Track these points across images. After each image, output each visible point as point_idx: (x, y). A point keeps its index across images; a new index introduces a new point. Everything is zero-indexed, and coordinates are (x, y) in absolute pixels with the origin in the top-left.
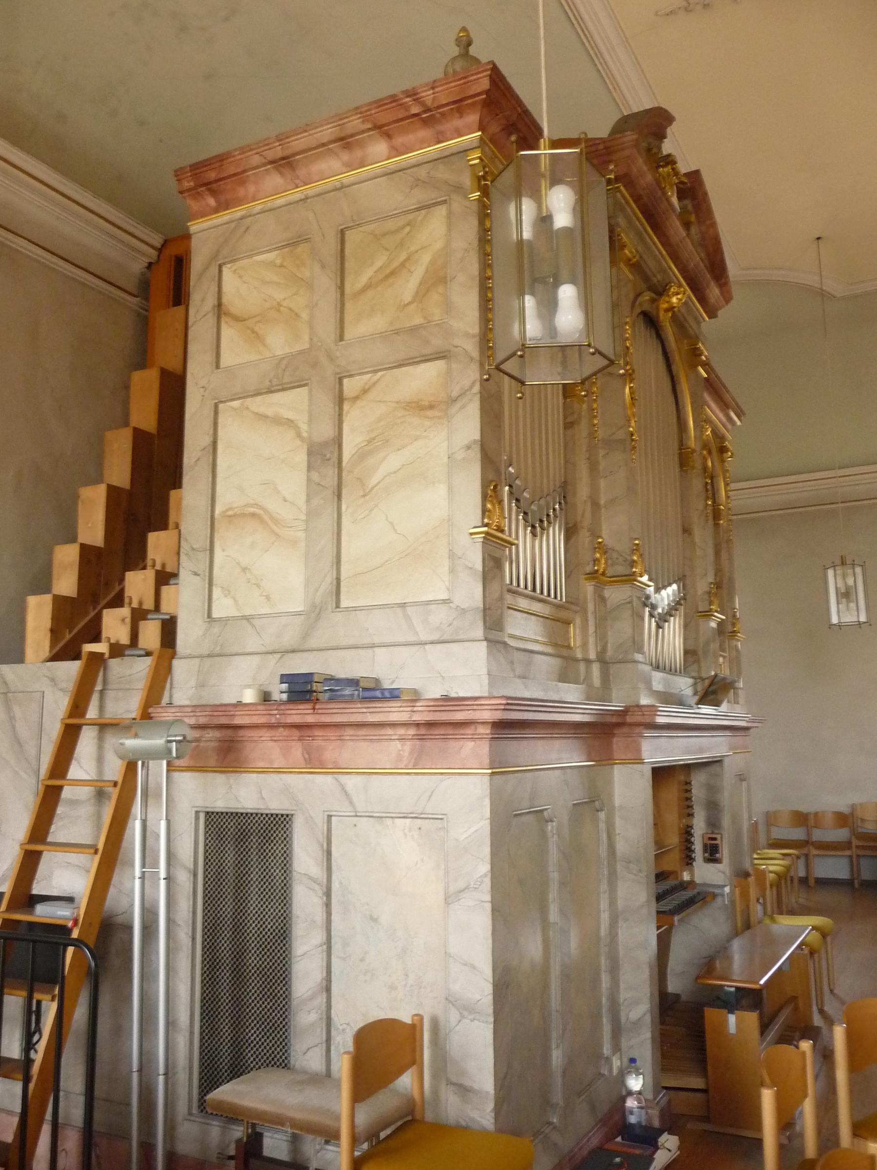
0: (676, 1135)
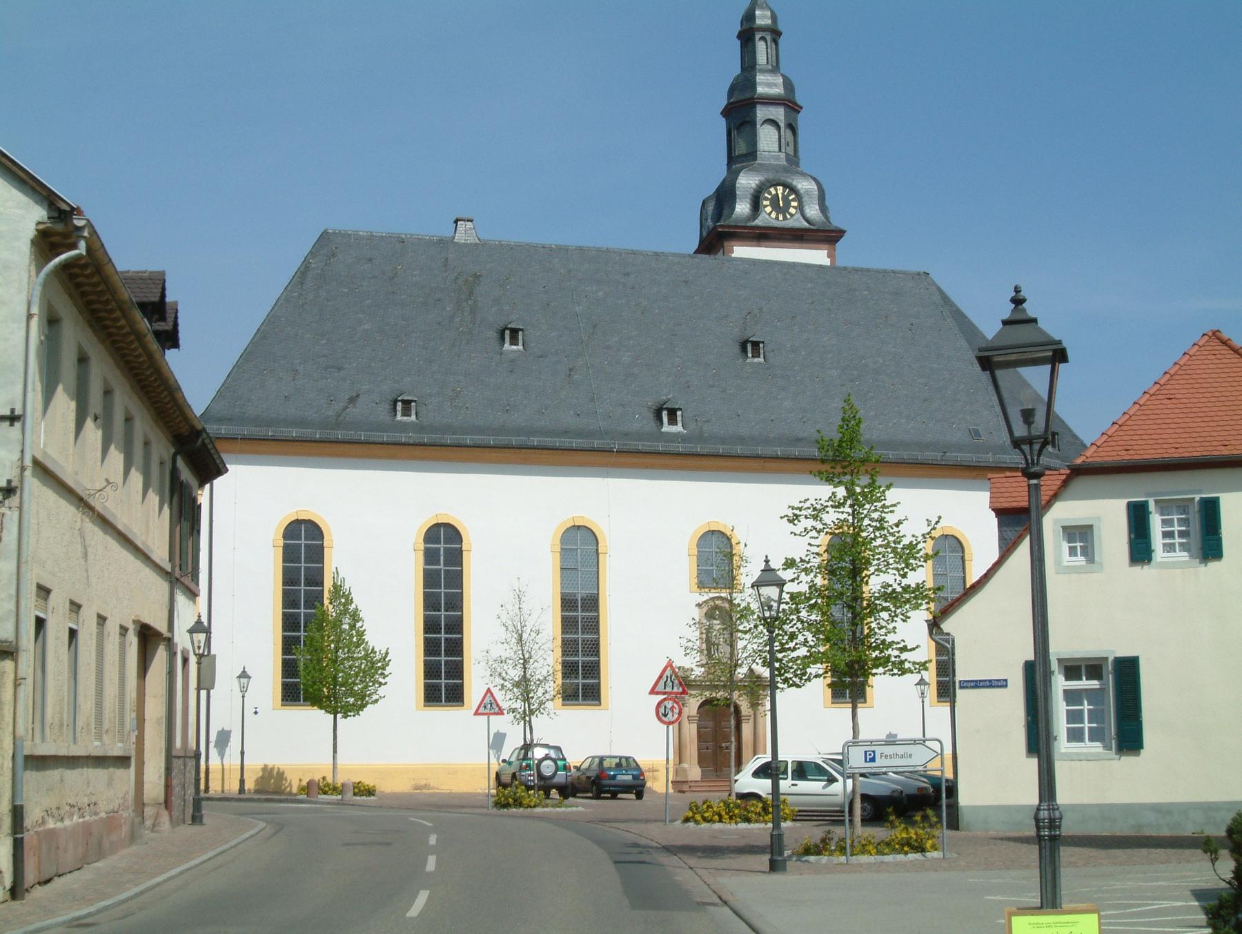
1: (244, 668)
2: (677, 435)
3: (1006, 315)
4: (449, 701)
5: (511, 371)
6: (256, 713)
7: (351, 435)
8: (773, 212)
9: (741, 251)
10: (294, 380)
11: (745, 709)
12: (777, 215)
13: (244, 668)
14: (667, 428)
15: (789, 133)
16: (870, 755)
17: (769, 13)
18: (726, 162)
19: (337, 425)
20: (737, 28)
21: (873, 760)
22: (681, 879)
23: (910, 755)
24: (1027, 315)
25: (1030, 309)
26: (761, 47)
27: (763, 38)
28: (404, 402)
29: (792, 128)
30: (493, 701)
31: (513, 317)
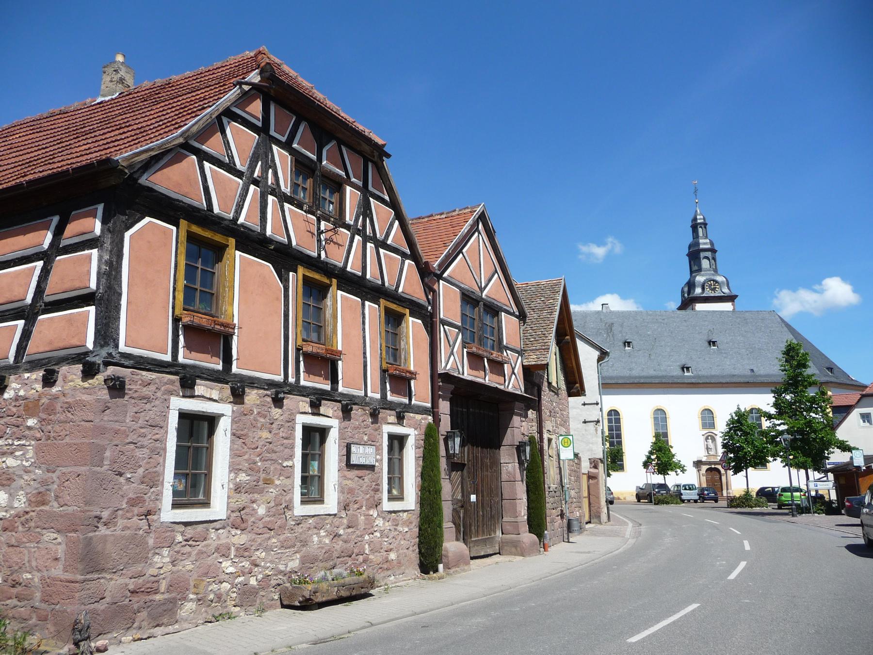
0: (144, 218)
2: (690, 376)
9: (700, 307)
11: (723, 471)
14: (686, 374)
15: (713, 261)
17: (702, 217)
18: (689, 272)
20: (690, 224)
26: (700, 230)
27: (701, 227)
29: (714, 259)
31: (627, 338)
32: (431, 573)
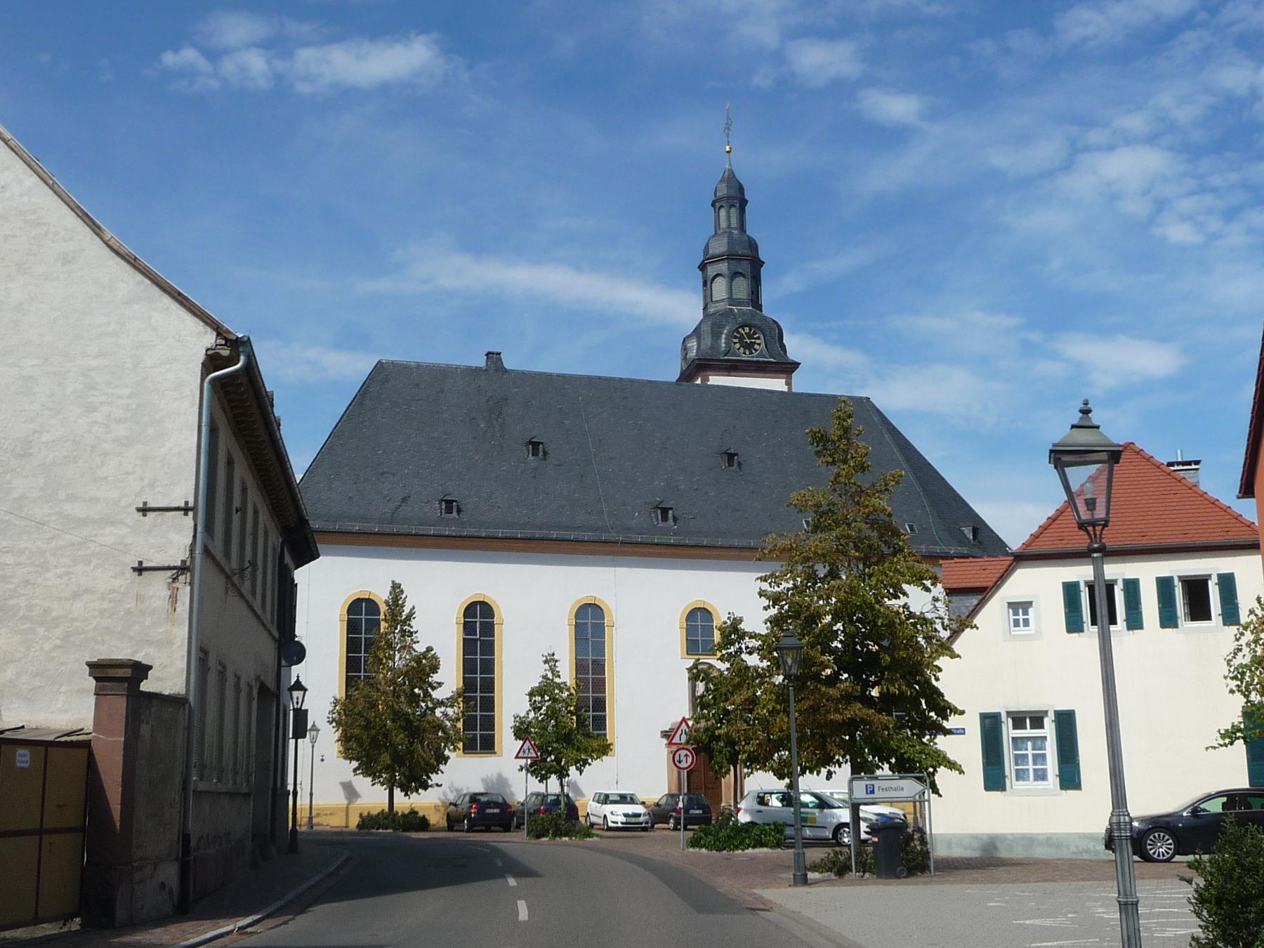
1: (314, 722)
3: (1075, 422)
4: (484, 749)
5: (534, 477)
6: (322, 760)
7: (404, 529)
8: (742, 348)
10: (356, 483)
12: (745, 350)
13: (314, 722)
16: (870, 788)
19: (392, 520)
21: (872, 792)
22: (722, 890)
23: (902, 789)
24: (1092, 422)
25: (1095, 418)
28: (446, 501)
30: (531, 747)
31: (535, 433)
32: (841, 721)
